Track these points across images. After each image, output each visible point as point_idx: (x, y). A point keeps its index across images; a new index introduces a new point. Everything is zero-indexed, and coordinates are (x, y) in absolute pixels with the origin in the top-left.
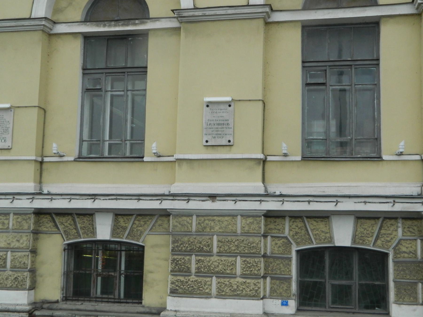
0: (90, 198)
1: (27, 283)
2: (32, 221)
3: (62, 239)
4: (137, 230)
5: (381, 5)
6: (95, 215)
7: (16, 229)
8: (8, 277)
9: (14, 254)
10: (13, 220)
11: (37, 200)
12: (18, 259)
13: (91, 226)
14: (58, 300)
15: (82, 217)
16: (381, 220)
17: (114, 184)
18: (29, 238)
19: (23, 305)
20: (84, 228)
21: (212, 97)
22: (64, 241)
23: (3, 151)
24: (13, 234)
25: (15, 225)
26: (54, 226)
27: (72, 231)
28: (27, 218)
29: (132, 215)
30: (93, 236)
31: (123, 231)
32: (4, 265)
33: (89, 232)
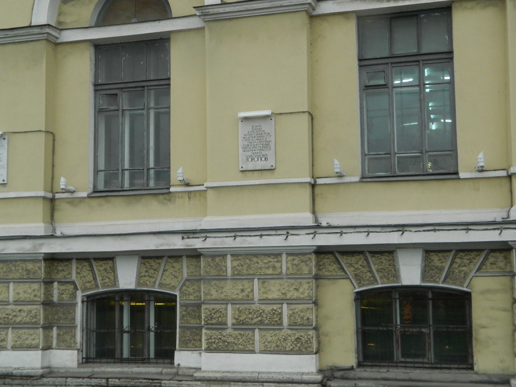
0: (396, 230)
1: (313, 344)
2: (314, 263)
3: (352, 285)
4: (460, 272)
5: (174, 18)
6: (115, 260)
7: (291, 274)
8: (287, 337)
9: (293, 307)
10: (287, 262)
11: (321, 235)
12: (299, 313)
13: (392, 268)
14: (353, 366)
15: (379, 255)
16: (453, 253)
17: (418, 210)
18: (312, 286)
19: (310, 374)
20: (383, 271)
21: (254, 111)
22: (355, 288)
23: (263, 172)
24: (289, 280)
25: (291, 269)
26: (340, 269)
27: (366, 274)
28: (307, 259)
29: (450, 251)
30: (395, 281)
31: (439, 273)
32: (280, 321)
33: (390, 275)
